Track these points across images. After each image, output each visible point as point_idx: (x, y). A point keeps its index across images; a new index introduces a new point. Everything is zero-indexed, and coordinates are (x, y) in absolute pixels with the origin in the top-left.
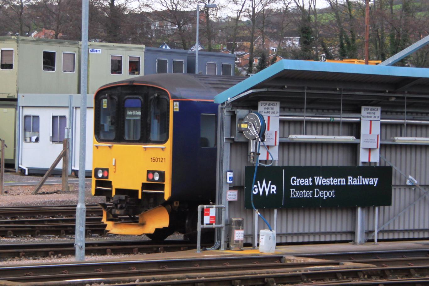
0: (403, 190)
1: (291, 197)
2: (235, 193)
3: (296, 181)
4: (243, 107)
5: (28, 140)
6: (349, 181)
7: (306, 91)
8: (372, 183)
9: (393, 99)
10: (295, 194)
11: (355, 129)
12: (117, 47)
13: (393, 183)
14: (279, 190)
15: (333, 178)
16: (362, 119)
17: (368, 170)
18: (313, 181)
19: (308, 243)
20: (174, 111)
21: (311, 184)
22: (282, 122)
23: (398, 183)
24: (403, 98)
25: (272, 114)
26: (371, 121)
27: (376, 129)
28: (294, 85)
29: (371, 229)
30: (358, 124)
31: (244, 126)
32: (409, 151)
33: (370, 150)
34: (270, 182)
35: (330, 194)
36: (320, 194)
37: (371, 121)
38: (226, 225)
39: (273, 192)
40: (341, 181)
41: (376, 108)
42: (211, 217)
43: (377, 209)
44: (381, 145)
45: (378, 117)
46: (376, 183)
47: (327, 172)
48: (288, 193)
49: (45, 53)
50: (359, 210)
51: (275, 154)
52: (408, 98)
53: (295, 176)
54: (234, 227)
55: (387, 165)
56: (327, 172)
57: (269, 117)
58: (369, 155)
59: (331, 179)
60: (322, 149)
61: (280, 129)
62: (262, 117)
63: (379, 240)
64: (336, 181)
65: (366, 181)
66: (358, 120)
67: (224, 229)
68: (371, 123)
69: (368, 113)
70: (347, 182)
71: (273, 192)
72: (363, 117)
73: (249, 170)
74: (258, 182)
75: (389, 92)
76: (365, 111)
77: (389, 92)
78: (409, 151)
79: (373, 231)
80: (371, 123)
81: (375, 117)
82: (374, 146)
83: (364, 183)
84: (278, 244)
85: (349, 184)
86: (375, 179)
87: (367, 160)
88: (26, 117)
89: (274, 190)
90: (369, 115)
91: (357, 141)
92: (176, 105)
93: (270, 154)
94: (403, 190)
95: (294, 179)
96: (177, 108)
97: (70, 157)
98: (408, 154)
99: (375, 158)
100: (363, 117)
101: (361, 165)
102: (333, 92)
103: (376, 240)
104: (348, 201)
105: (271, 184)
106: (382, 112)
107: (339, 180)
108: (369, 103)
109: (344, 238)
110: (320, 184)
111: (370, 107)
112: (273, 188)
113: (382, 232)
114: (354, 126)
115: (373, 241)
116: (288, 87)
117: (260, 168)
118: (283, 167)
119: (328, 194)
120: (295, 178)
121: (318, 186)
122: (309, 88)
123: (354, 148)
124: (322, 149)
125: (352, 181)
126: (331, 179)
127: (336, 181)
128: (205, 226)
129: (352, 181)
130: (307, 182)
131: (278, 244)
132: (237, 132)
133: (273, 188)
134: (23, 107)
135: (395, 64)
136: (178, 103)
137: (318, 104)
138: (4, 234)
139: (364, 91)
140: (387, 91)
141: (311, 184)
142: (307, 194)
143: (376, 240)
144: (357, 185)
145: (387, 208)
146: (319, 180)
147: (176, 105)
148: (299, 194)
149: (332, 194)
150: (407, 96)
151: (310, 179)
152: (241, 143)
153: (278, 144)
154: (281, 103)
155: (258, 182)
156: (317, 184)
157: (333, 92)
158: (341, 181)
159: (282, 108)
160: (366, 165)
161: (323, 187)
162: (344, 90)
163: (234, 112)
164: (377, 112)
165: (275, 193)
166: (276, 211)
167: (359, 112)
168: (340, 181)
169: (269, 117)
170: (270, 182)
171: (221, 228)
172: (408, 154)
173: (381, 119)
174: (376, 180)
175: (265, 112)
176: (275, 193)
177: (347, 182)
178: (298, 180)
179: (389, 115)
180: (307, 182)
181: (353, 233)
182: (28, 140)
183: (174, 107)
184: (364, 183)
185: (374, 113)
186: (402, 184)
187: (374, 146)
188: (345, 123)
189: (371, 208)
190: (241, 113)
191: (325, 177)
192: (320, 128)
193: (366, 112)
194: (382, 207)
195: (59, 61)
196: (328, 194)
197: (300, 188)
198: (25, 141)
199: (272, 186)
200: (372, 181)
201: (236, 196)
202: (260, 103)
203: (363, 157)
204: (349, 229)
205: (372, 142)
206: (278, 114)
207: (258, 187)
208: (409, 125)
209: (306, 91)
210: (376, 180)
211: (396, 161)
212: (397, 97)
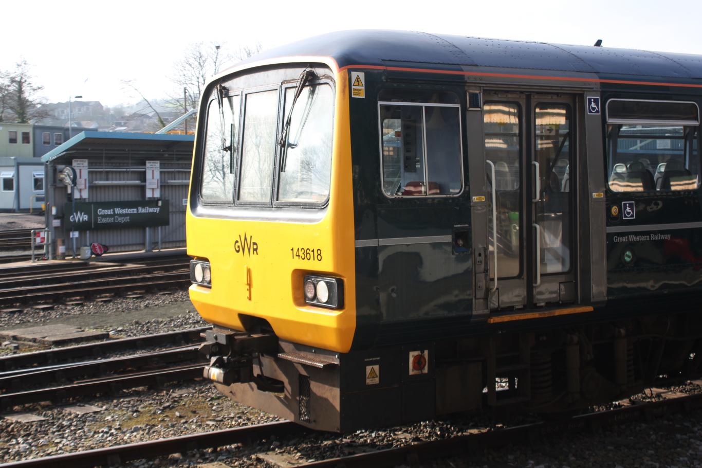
0: (178, 215)
3: (101, 212)
4: (62, 164)
7: (104, 152)
9: (167, 155)
10: (102, 221)
11: (142, 176)
13: (170, 210)
14: (90, 218)
15: (129, 209)
16: (147, 169)
17: (153, 202)
18: (114, 211)
20: (353, 96)
21: (112, 213)
23: (174, 210)
24: (173, 154)
25: (82, 167)
26: (153, 171)
27: (157, 175)
29: (157, 241)
30: (144, 173)
31: (62, 176)
32: (118, 190)
33: (153, 189)
34: (83, 213)
36: (119, 220)
37: (153, 171)
40: (134, 211)
41: (156, 161)
46: (158, 211)
50: (147, 229)
51: (85, 195)
52: (176, 155)
55: (167, 199)
57: (80, 170)
58: (153, 191)
60: (120, 190)
61: (88, 177)
62: (74, 171)
64: (130, 211)
68: (153, 171)
69: (151, 165)
70: (650, 238)
72: (148, 168)
75: (163, 151)
77: (163, 151)
78: (118, 190)
80: (153, 171)
82: (155, 186)
85: (652, 239)
91: (143, 184)
92: (358, 80)
93: (82, 193)
94: (178, 215)
95: (100, 211)
96: (360, 90)
98: (181, 192)
99: (157, 194)
100: (148, 168)
101: (147, 199)
102: (124, 152)
104: (138, 224)
107: (132, 210)
110: (79, 214)
120: (101, 210)
121: (117, 215)
122: (106, 150)
123: (143, 189)
124: (120, 190)
125: (141, 210)
126: (127, 210)
127: (130, 211)
128: (37, 244)
129: (141, 210)
132: (58, 181)
136: (362, 75)
142: (110, 220)
145: (167, 227)
146: (118, 211)
147: (358, 80)
148: (104, 220)
149: (128, 219)
150: (175, 153)
155: (75, 214)
156: (116, 213)
157: (124, 152)
158: (134, 211)
161: (120, 215)
162: (132, 151)
167: (145, 164)
168: (133, 211)
169: (80, 170)
172: (181, 192)
173: (160, 169)
175: (77, 167)
177: (650, 238)
178: (103, 211)
180: (110, 212)
183: (353, 87)
186: (177, 210)
187: (155, 186)
188: (133, 172)
189: (156, 228)
190: (60, 167)
192: (118, 175)
193: (76, 163)
194: (164, 227)
202: (73, 161)
203: (149, 194)
204: (141, 242)
206: (87, 168)
208: (179, 172)
209: (104, 152)
212: (169, 154)
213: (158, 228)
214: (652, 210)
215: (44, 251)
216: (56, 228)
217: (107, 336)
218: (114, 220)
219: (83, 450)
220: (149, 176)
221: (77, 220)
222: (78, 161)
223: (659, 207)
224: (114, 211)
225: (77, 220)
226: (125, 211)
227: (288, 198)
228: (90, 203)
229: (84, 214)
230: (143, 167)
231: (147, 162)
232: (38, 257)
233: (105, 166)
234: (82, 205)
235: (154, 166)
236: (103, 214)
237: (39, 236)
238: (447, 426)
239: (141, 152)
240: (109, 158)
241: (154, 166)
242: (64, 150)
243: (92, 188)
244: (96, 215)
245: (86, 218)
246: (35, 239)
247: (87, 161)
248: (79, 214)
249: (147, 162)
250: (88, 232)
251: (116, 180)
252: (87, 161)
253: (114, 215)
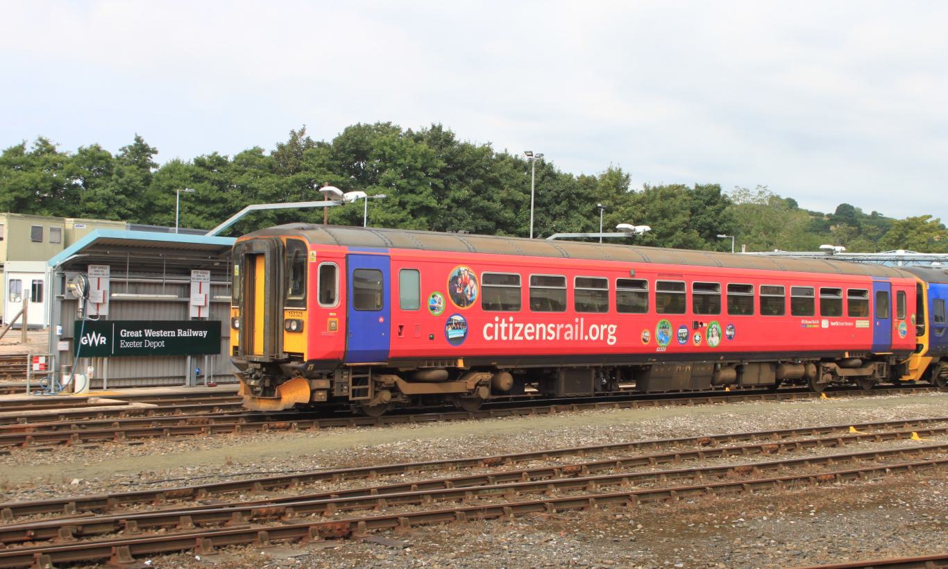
1: (121, 347)
2: (67, 343)
3: (125, 333)
5: (13, 300)
6: (179, 333)
9: (217, 264)
10: (123, 344)
12: (16, 217)
14: (109, 341)
17: (198, 324)
18: (143, 333)
19: (232, 383)
21: (141, 336)
22: (212, 286)
26: (99, 278)
27: (206, 288)
28: (199, 255)
30: (189, 285)
31: (73, 286)
34: (99, 335)
35: (160, 344)
36: (150, 344)
37: (99, 278)
38: (56, 371)
40: (173, 334)
41: (105, 266)
42: (41, 364)
43: (206, 357)
44: (211, 303)
46: (205, 335)
47: (157, 325)
48: (117, 344)
49: (33, 227)
50: (189, 358)
51: (104, 311)
53: (614, 324)
54: (64, 373)
56: (157, 325)
59: (161, 331)
63: (108, 388)
64: (166, 334)
65: (195, 333)
66: (188, 281)
67: (53, 375)
70: (177, 333)
72: (193, 279)
73: (78, 324)
74: (88, 335)
76: (194, 274)
77: (212, 258)
79: (203, 376)
81: (104, 275)
82: (202, 303)
84: (91, 388)
87: (197, 316)
88: (11, 280)
90: (96, 273)
95: (123, 332)
99: (205, 314)
100: (193, 279)
103: (105, 388)
104: (176, 350)
106: (211, 274)
107: (169, 332)
108: (198, 268)
109: (176, 382)
110: (94, 335)
111: (200, 271)
113: (108, 380)
114: (186, 287)
115: (203, 384)
116: (110, 253)
117: (87, 322)
118: (113, 322)
119: (158, 344)
120: (125, 331)
125: (180, 333)
126: (161, 331)
127: (166, 334)
129: (180, 333)
130: (138, 334)
131: (91, 388)
132: (66, 291)
134: (8, 272)
135: (221, 234)
137: (137, 268)
138: (5, 377)
139: (186, 257)
141: (141, 336)
142: (138, 345)
143: (105, 388)
144: (187, 337)
146: (149, 333)
148: (128, 345)
151: (140, 332)
152: (69, 301)
153: (208, 304)
154: (111, 266)
155: (88, 335)
156: (146, 335)
158: (173, 334)
160: (196, 320)
163: (64, 274)
164: (207, 274)
166: (189, 358)
167: (189, 274)
168: (170, 334)
170: (99, 335)
171: (51, 374)
174: (205, 333)
178: (128, 332)
179: (216, 278)
180: (138, 334)
181: (184, 377)
182: (13, 300)
190: (68, 274)
191: (156, 329)
193: (196, 274)
195: (47, 234)
196: (158, 344)
197: (129, 339)
198: (10, 300)
199: (102, 338)
201: (68, 346)
205: (830, 308)
206: (108, 276)
207: (87, 339)
210: (205, 333)
215: (44, 382)
216: (62, 352)
217: (663, 392)
218: (143, 344)
219: (568, 477)
220: (194, 287)
222: (198, 272)
224: (143, 333)
229: (101, 336)
230: (187, 277)
231: (193, 271)
232: (34, 388)
236: (128, 336)
237: (37, 362)
238: (717, 524)
241: (100, 273)
242: (74, 252)
243: (113, 303)
244: (118, 338)
245: (103, 340)
246: (31, 366)
247: (209, 272)
248: (94, 335)
249: (89, 267)
251: (160, 294)
252: (209, 272)
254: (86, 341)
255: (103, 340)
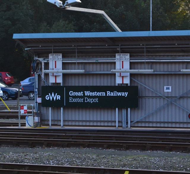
3: (72, 93)
8: (124, 95)
14: (62, 98)
17: (122, 88)
18: (84, 94)
21: (82, 95)
34: (56, 94)
39: (58, 99)
40: (104, 94)
45: (61, 59)
46: (126, 95)
64: (99, 94)
65: (119, 94)
71: (58, 99)
74: (49, 94)
83: (118, 95)
86: (125, 93)
89: (59, 98)
95: (71, 93)
97: (173, 68)
99: (127, 81)
105: (57, 95)
107: (101, 93)
110: (53, 94)
112: (59, 97)
120: (72, 92)
121: (87, 96)
127: (99, 94)
129: (109, 93)
133: (59, 97)
140: (73, 46)
142: (81, 100)
146: (87, 93)
148: (74, 100)
155: (49, 94)
156: (86, 95)
157: (38, 48)
158: (104, 94)
159: (63, 57)
161: (89, 97)
165: (60, 99)
168: (102, 94)
170: (56, 94)
174: (126, 94)
176: (60, 99)
178: (74, 93)
184: (118, 95)
185: (58, 57)
199: (58, 96)
200: (124, 94)
207: (49, 96)
210: (126, 94)
211: (140, 83)
213: (49, 108)
214: (36, 109)
218: (84, 100)
221: (51, 99)
223: (71, 92)
224: (84, 94)
225: (51, 99)
226: (93, 94)
227: (134, 78)
228: (63, 87)
231: (117, 54)
233: (77, 58)
234: (56, 88)
235: (56, 58)
237: (23, 109)
239: (160, 46)
240: (148, 52)
241: (56, 58)
244: (68, 96)
245: (59, 97)
247: (129, 54)
248: (53, 94)
250: (50, 108)
253: (84, 96)
254: (48, 97)
255: (59, 97)
